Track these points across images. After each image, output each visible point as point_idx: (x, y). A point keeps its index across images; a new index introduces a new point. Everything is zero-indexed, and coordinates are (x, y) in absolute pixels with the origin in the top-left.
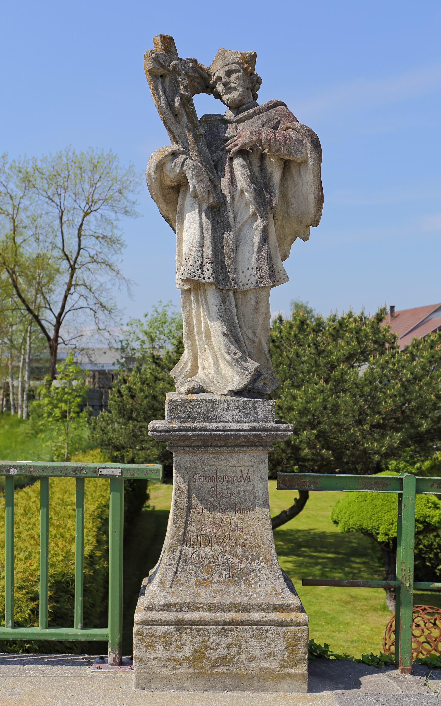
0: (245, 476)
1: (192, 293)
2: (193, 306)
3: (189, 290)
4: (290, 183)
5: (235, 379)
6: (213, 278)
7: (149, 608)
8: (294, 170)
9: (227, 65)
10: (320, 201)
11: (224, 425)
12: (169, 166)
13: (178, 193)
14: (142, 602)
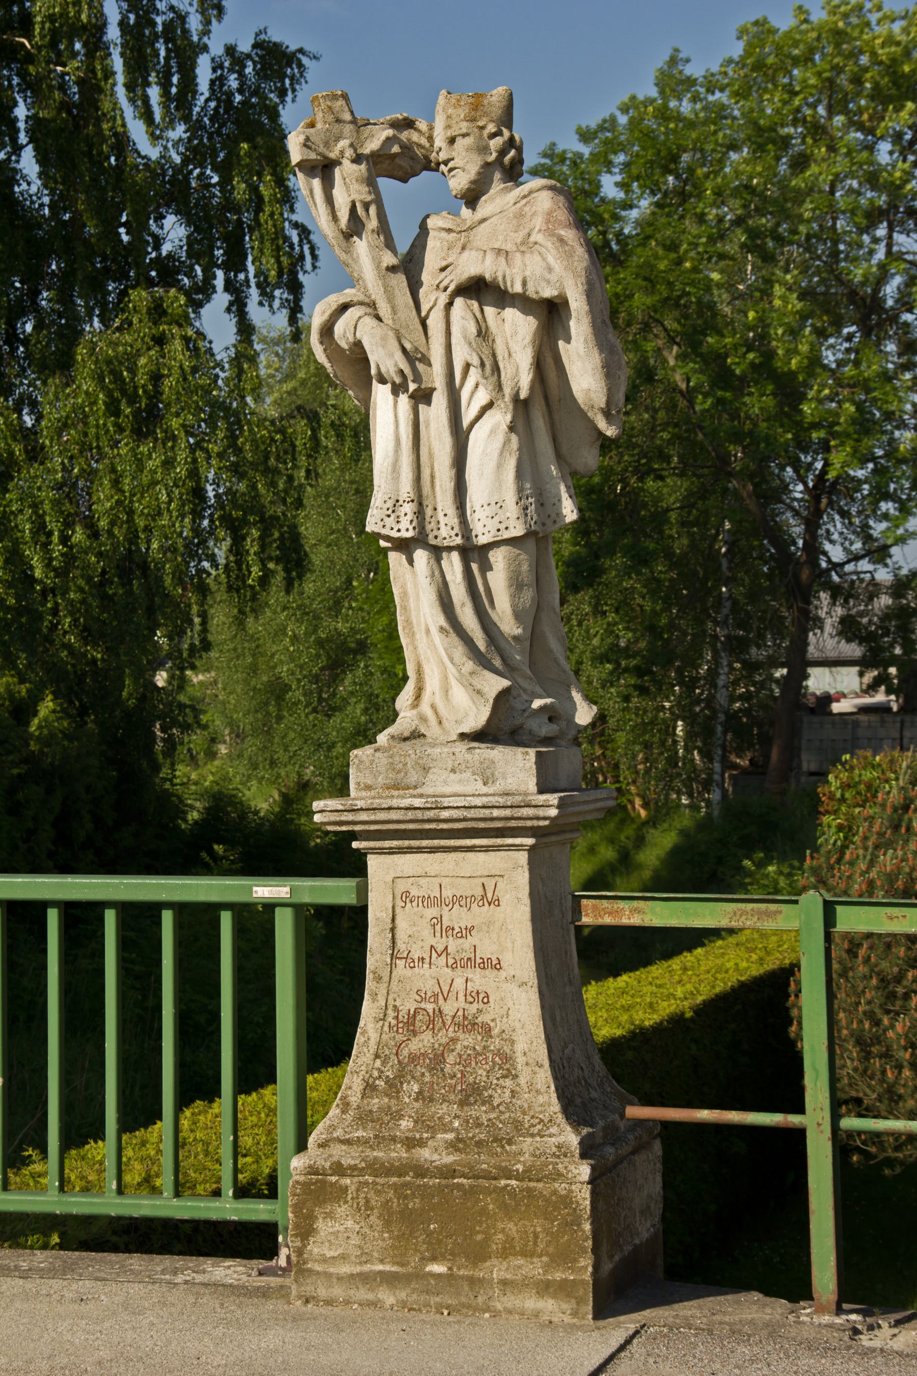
0: (490, 895)
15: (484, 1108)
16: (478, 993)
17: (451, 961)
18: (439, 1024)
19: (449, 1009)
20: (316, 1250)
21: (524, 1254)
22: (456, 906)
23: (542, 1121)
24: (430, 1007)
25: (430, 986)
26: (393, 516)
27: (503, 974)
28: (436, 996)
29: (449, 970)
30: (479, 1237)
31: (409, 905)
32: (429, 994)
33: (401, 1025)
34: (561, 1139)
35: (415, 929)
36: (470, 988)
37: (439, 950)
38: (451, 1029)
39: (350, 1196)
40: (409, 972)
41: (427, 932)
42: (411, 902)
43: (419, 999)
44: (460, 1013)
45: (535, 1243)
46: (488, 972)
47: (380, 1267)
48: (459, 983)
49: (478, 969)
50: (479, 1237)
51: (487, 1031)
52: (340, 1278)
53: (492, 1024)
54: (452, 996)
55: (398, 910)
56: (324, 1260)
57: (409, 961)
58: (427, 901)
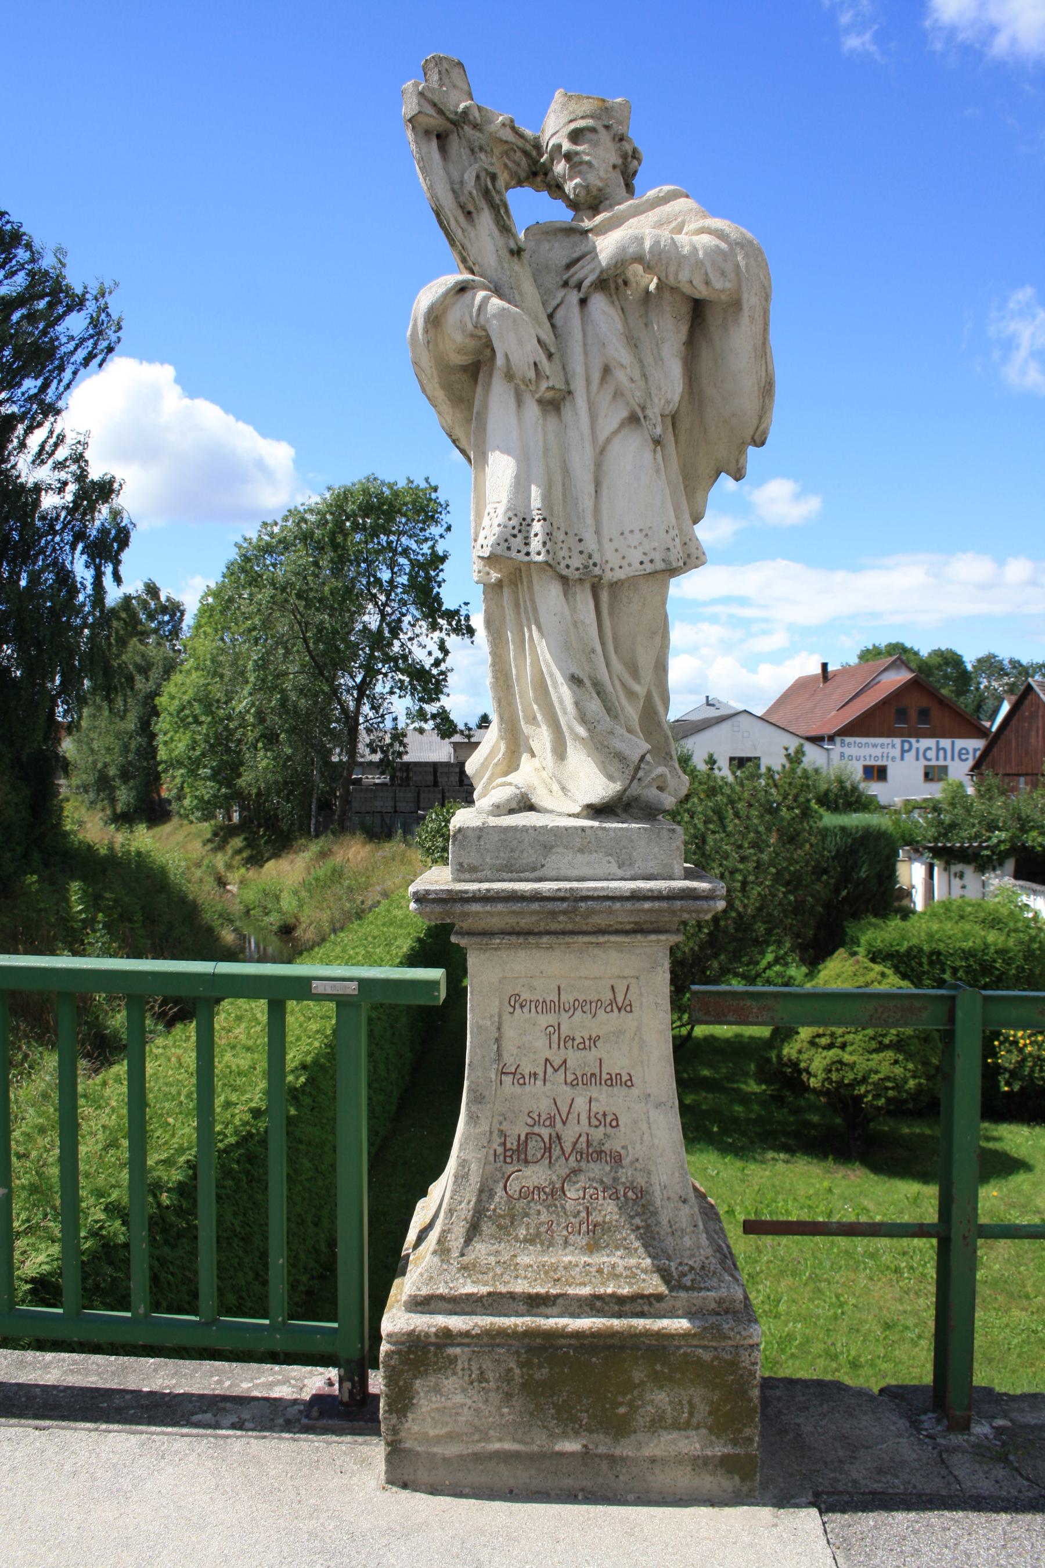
0: (620, 1000)
1: (506, 591)
2: (508, 617)
3: (499, 585)
4: (705, 353)
5: (593, 784)
6: (548, 551)
7: (421, 1304)
8: (714, 319)
9: (571, 121)
10: (767, 389)
11: (575, 885)
12: (454, 316)
13: (476, 381)
14: (404, 1288)
15: (619, 1253)
16: (605, 1115)
17: (570, 1077)
18: (556, 1152)
19: (569, 1135)
20: (416, 1428)
21: (676, 1426)
22: (579, 1012)
23: (692, 1268)
24: (545, 1132)
25: (545, 1106)
26: (520, 536)
27: (635, 1091)
28: (552, 1118)
29: (568, 1089)
30: (622, 1410)
31: (518, 1010)
32: (544, 1117)
33: (508, 1153)
34: (723, 1292)
35: (528, 1039)
36: (594, 1109)
37: (557, 1063)
38: (572, 1159)
39: (459, 1367)
40: (518, 1090)
41: (541, 1043)
42: (522, 1006)
43: (530, 1121)
44: (583, 1139)
45: (691, 1414)
46: (616, 1090)
47: (497, 1446)
48: (581, 1103)
49: (605, 1087)
50: (622, 1410)
51: (617, 1159)
52: (446, 1460)
53: (623, 1152)
54: (573, 1116)
55: (506, 1017)
56: (425, 1438)
57: (518, 1076)
58: (543, 1006)
